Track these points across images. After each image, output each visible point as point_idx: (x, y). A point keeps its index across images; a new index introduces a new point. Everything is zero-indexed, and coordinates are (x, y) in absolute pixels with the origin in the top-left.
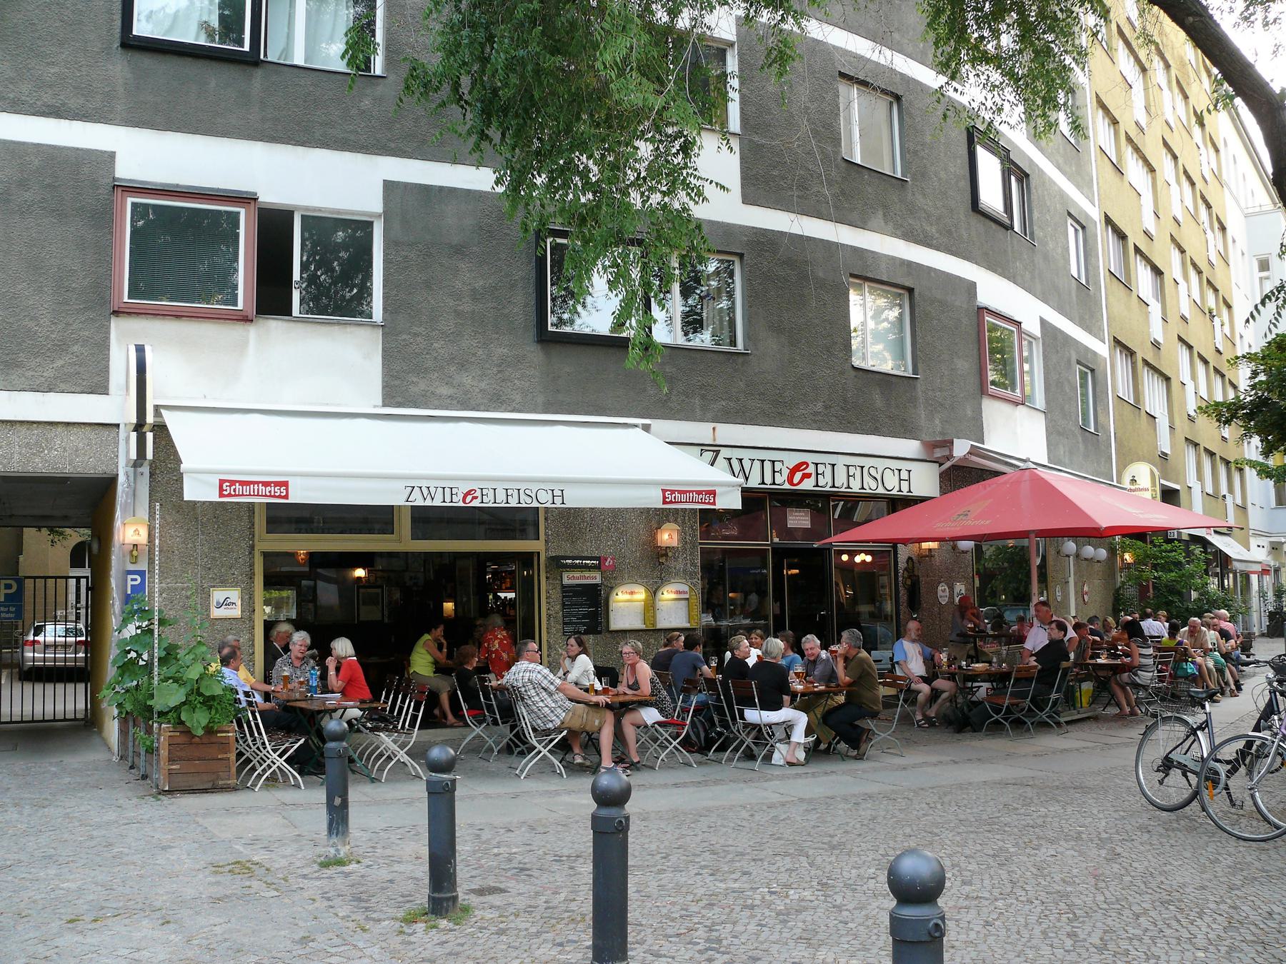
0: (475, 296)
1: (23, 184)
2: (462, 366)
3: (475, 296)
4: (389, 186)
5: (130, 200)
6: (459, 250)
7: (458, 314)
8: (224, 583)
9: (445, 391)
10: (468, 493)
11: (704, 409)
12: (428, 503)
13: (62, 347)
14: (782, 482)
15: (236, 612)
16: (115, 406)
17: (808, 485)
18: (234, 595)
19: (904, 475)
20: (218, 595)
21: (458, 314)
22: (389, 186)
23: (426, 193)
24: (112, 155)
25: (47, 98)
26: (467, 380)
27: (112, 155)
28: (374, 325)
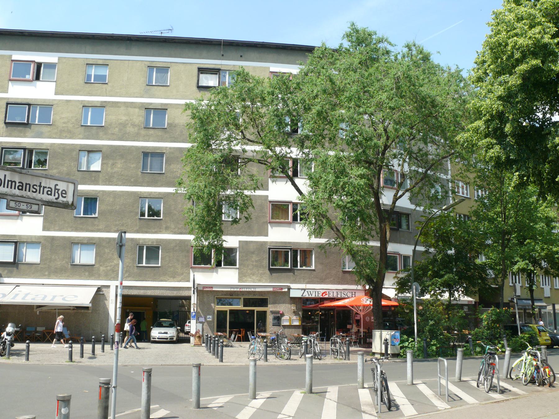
0: (256, 261)
1: (176, 246)
2: (253, 275)
3: (256, 261)
4: (240, 242)
5: (160, 265)
6: (253, 253)
7: (253, 265)
8: (209, 315)
9: (250, 280)
10: (324, 293)
11: (304, 281)
12: (310, 296)
13: (182, 274)
14: (320, 296)
15: (211, 320)
16: (190, 284)
17: (327, 296)
18: (211, 317)
19: (353, 293)
20: (208, 317)
21: (253, 265)
22: (240, 242)
23: (247, 242)
24: (268, 190)
25: (180, 231)
26: (254, 277)
27: (268, 190)
28: (237, 268)
